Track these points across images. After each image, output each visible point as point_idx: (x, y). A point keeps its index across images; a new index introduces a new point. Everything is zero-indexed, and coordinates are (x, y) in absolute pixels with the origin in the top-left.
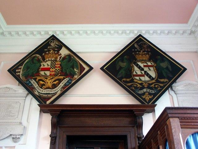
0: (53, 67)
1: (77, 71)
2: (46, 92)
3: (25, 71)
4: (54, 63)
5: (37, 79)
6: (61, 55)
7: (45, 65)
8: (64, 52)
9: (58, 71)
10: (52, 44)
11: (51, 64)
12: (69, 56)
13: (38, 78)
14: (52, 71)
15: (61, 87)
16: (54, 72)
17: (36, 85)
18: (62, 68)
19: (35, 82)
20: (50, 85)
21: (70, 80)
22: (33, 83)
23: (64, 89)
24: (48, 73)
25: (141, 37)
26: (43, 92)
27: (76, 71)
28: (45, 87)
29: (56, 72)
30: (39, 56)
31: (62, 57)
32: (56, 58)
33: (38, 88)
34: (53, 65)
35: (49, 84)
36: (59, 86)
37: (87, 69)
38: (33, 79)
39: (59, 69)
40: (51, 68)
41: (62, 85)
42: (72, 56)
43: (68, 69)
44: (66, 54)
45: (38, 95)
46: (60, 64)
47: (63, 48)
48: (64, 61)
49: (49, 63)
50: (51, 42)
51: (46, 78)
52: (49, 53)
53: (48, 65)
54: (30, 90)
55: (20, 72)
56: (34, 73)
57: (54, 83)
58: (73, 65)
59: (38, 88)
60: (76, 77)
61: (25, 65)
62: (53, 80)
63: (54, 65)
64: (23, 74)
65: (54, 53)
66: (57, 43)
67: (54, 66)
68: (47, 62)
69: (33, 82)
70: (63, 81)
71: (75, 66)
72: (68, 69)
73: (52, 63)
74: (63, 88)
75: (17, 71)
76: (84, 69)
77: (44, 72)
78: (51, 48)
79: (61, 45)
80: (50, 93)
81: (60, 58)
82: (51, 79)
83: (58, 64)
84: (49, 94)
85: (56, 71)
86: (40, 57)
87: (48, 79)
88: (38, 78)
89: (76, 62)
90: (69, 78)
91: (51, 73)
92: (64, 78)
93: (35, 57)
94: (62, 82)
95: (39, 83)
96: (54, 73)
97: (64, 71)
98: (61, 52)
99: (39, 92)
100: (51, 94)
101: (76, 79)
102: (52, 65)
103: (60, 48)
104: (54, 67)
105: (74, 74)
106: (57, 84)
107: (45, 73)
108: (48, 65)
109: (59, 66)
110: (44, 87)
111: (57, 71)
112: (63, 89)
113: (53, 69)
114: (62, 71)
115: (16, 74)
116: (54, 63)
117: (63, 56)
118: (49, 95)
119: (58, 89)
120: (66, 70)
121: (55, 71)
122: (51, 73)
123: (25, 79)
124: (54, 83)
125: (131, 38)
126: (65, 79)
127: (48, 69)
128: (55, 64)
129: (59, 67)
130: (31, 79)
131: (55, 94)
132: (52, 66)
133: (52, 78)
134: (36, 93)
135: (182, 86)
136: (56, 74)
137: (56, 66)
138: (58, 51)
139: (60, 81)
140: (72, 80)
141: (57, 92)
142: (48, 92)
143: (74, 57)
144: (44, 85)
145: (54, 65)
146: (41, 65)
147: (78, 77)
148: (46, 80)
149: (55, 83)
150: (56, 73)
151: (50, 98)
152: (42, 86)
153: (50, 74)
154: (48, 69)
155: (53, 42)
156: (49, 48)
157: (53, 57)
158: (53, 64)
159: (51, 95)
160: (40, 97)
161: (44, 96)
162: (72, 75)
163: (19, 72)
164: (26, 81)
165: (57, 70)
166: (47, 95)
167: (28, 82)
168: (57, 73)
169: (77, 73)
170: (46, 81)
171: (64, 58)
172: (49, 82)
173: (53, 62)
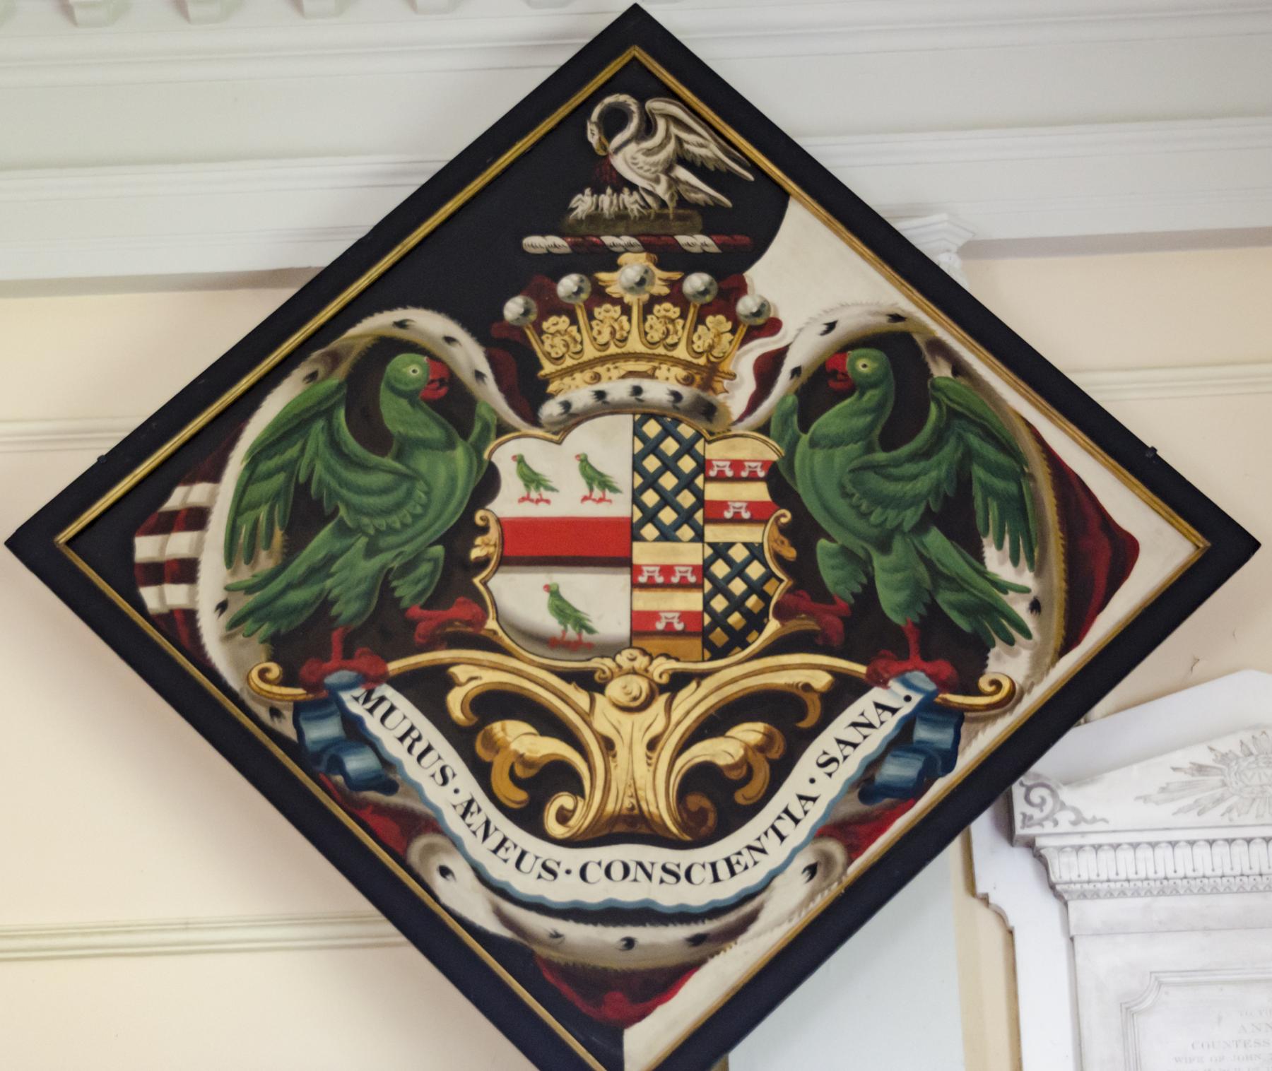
0: (668, 516)
1: (1026, 578)
2: (596, 893)
3: (266, 562)
4: (687, 448)
5: (450, 683)
6: (768, 325)
7: (560, 470)
8: (812, 284)
9: (755, 571)
10: (630, 158)
11: (637, 466)
12: (893, 342)
13: (472, 674)
14: (667, 580)
15: (816, 812)
16: (684, 585)
17: (438, 779)
18: (803, 532)
19: (430, 733)
20: (647, 782)
21: (930, 710)
22: (395, 749)
23: (853, 851)
24: (604, 600)
25: (636, 52)
26: (562, 891)
27: (1004, 587)
28: (582, 820)
29: (720, 587)
30: (453, 329)
31: (789, 364)
32: (709, 374)
33: (477, 820)
34: (668, 481)
35: (642, 771)
36: (785, 796)
37: (1163, 550)
38: (402, 683)
39: (755, 552)
40: (650, 531)
41: (829, 788)
42: (939, 348)
43: (885, 547)
44: (850, 323)
45: (493, 926)
46: (777, 478)
47: (802, 222)
48: (831, 421)
49: (610, 445)
50: (614, 122)
51: (591, 683)
52: (600, 295)
53: (596, 479)
54: (362, 839)
55: (205, 573)
56: (405, 590)
57: (704, 751)
58: (963, 482)
59: (477, 820)
60: (1008, 665)
61: (255, 457)
62: (692, 704)
63: (687, 482)
64: (241, 603)
65: (676, 295)
66: (704, 147)
67: (686, 499)
68: (583, 438)
69: (395, 723)
70: (840, 727)
71: (989, 513)
72: (884, 546)
73: (652, 447)
74: (845, 830)
75: (146, 548)
76: (1124, 551)
77: (554, 593)
78: (621, 220)
79: (762, 178)
80: (669, 896)
81: (768, 369)
82: (656, 690)
83: (738, 474)
84: (646, 914)
85: (720, 569)
86: (469, 356)
87: (615, 689)
88: (472, 674)
89: (1000, 435)
90: (919, 678)
91: (647, 601)
92: (844, 692)
93: (387, 347)
94: (825, 743)
95: (494, 746)
96: (692, 601)
97: (831, 573)
98: (766, 280)
99: (501, 891)
100: (682, 916)
101: (1014, 697)
102: (651, 482)
103: (745, 223)
104: (686, 517)
105: (989, 623)
106: (746, 768)
107: (561, 608)
108: (596, 479)
109: (759, 492)
110: (563, 817)
111: (738, 571)
112: (835, 849)
113: (667, 535)
114: (803, 571)
115: (140, 605)
116: (687, 448)
117: (803, 346)
118: (645, 935)
119: (777, 852)
120: (865, 565)
121: (704, 570)
122: (647, 601)
123: (286, 681)
124: (704, 751)
125: (544, 43)
126: (863, 706)
127: (597, 546)
128: (703, 465)
129: (758, 514)
130: (369, 681)
131: (733, 918)
132: (650, 498)
133: (678, 681)
134: (463, 898)
135: (1158, 773)
136: (719, 620)
137: (714, 492)
138: (729, 272)
139: (791, 722)
140: (957, 718)
141: (765, 885)
142: (629, 893)
143: (959, 368)
144: (558, 777)
145: (687, 482)
146: (488, 484)
147: (1039, 668)
148: (581, 698)
149: (723, 750)
150: (719, 603)
151: (661, 983)
152: (535, 796)
153: (642, 626)
154: (597, 546)
155: (648, 128)
156: (595, 218)
157: (655, 358)
158: (669, 465)
159: (681, 933)
160: (516, 952)
161: (654, 946)
162: (953, 642)
163: (186, 571)
164: (300, 709)
165: (739, 554)
166: (613, 935)
167: (322, 731)
168: (737, 604)
169: (1021, 608)
170: (586, 717)
171: (823, 385)
172: (632, 731)
173: (667, 432)
